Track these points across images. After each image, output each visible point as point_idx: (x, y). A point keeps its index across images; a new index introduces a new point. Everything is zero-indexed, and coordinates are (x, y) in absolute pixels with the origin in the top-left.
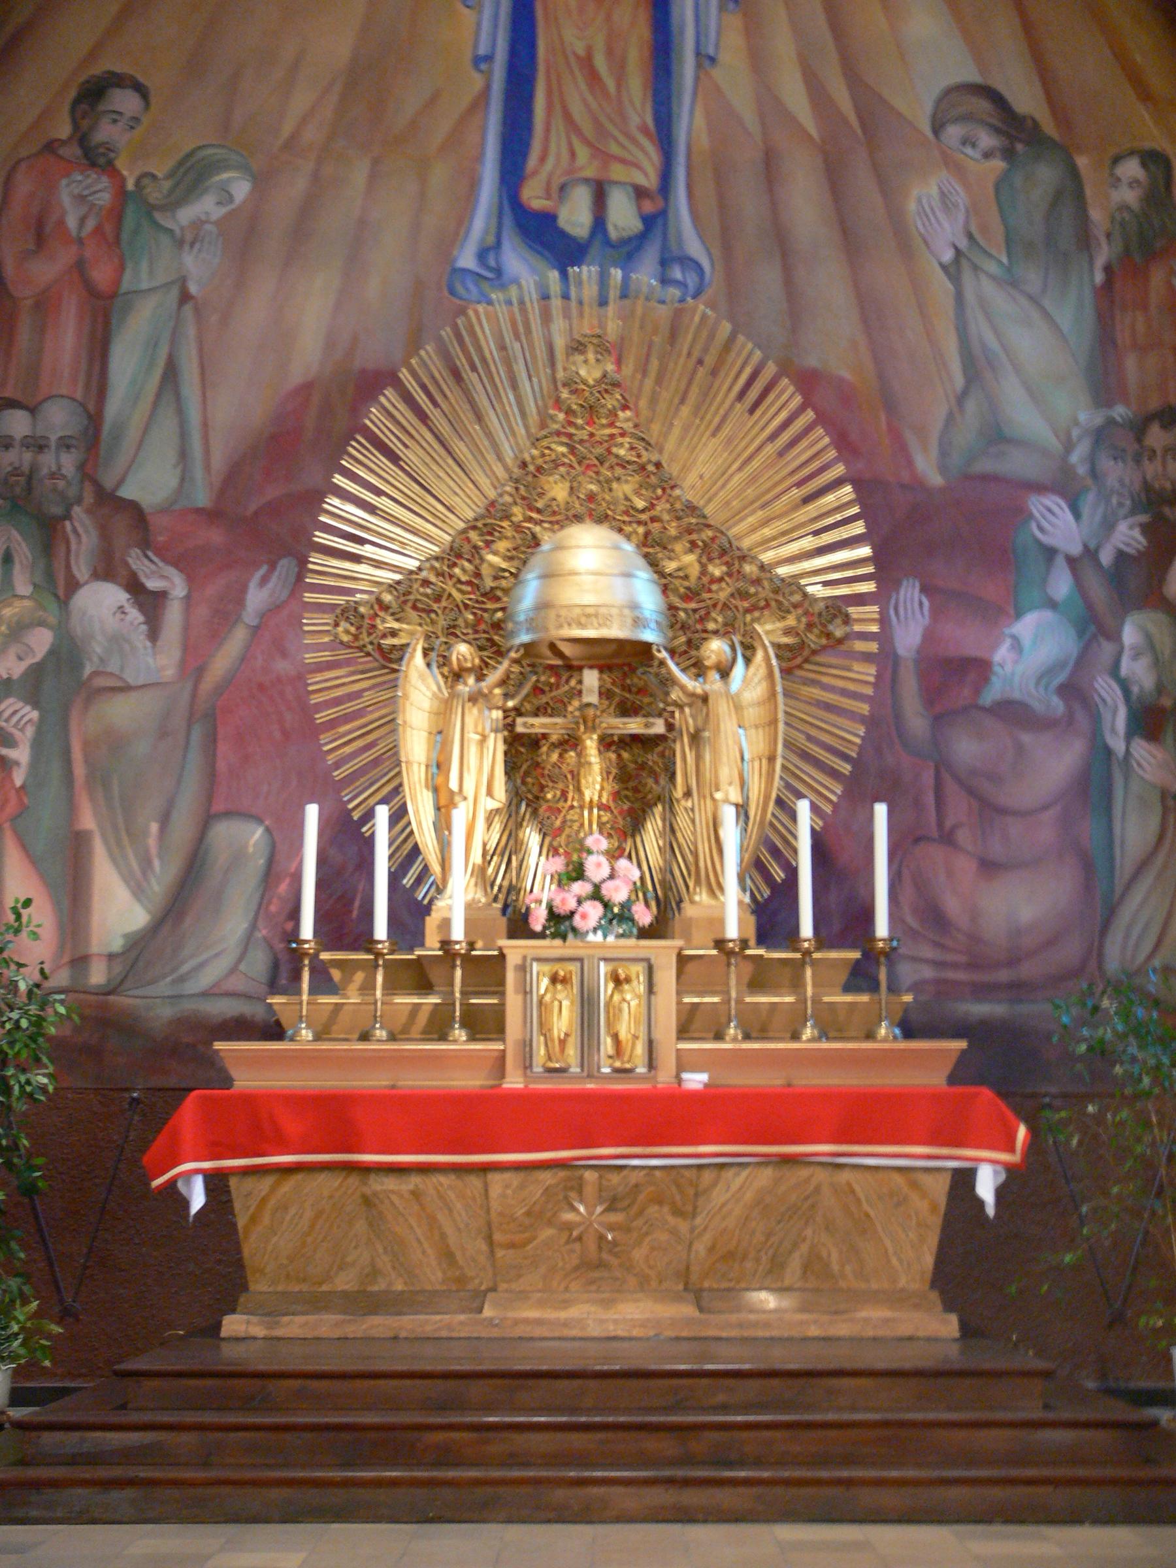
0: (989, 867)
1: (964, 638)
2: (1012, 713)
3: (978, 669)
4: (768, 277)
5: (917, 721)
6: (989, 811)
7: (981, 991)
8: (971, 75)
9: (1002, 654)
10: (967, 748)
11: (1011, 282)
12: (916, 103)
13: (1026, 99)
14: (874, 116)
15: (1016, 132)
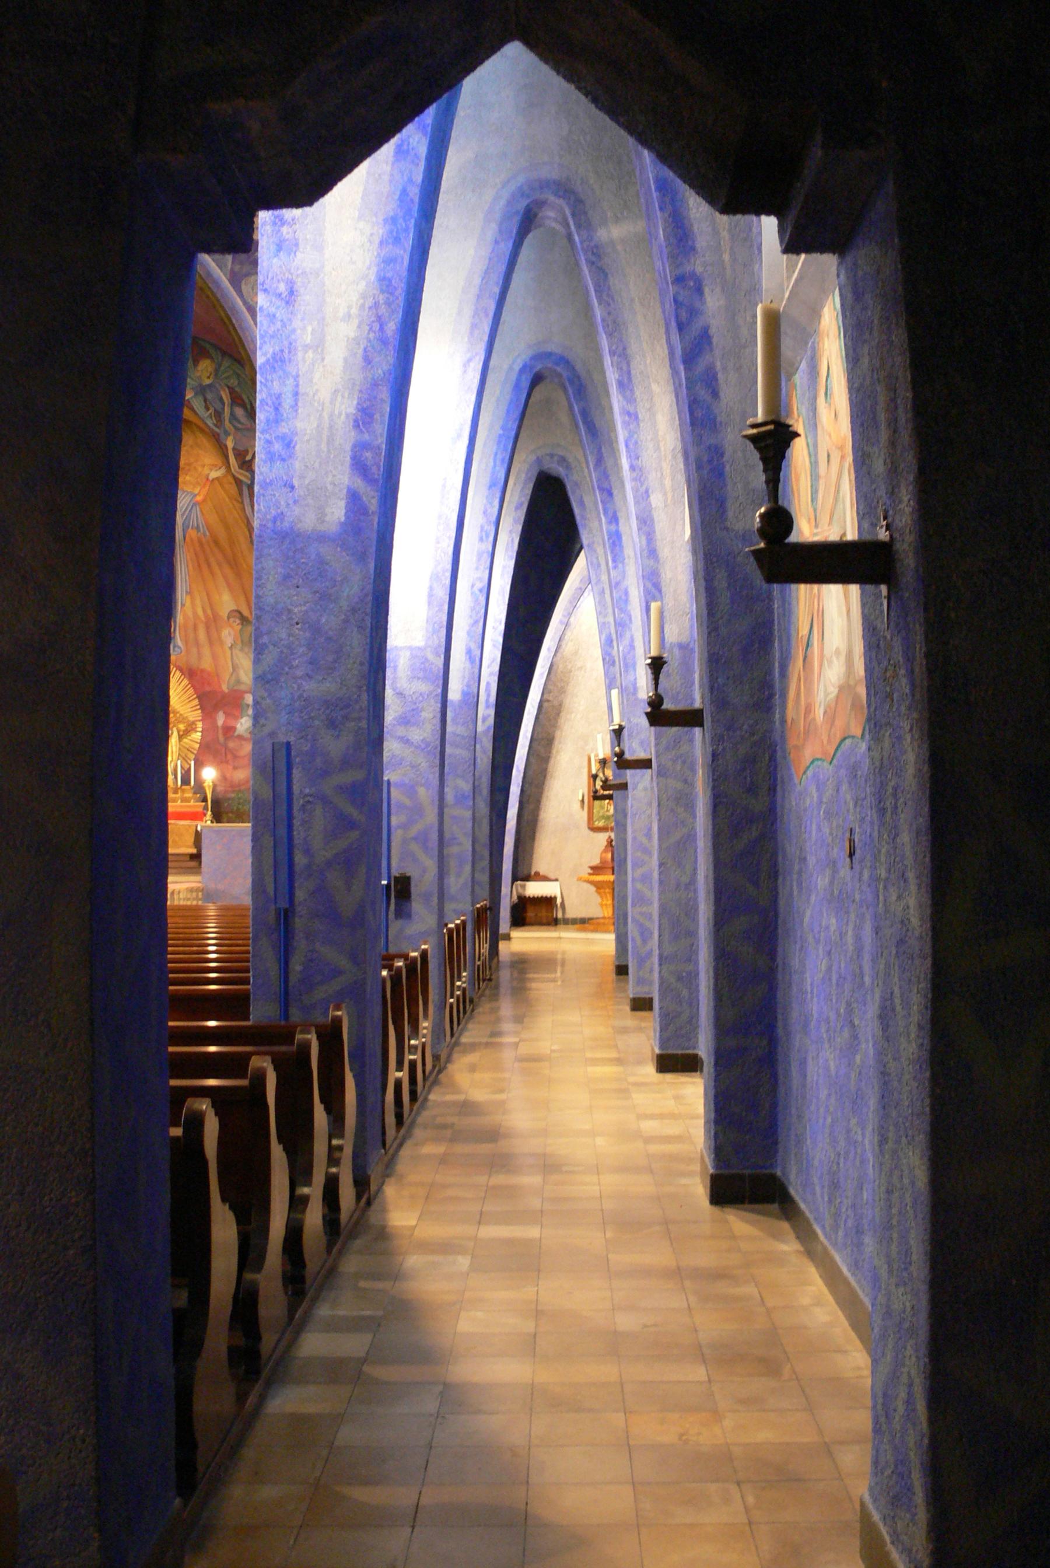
0: (235, 768)
1: (231, 723)
2: (240, 737)
3: (234, 729)
4: (194, 650)
5: (221, 739)
6: (235, 757)
7: (233, 792)
8: (234, 608)
9: (238, 726)
10: (231, 744)
11: (242, 650)
12: (224, 613)
13: (246, 613)
14: (216, 617)
15: (244, 620)
